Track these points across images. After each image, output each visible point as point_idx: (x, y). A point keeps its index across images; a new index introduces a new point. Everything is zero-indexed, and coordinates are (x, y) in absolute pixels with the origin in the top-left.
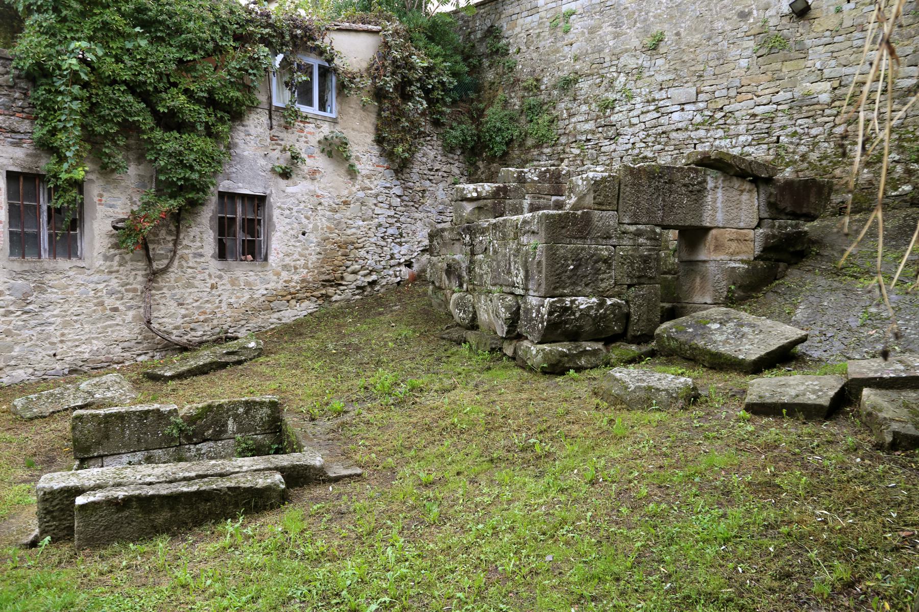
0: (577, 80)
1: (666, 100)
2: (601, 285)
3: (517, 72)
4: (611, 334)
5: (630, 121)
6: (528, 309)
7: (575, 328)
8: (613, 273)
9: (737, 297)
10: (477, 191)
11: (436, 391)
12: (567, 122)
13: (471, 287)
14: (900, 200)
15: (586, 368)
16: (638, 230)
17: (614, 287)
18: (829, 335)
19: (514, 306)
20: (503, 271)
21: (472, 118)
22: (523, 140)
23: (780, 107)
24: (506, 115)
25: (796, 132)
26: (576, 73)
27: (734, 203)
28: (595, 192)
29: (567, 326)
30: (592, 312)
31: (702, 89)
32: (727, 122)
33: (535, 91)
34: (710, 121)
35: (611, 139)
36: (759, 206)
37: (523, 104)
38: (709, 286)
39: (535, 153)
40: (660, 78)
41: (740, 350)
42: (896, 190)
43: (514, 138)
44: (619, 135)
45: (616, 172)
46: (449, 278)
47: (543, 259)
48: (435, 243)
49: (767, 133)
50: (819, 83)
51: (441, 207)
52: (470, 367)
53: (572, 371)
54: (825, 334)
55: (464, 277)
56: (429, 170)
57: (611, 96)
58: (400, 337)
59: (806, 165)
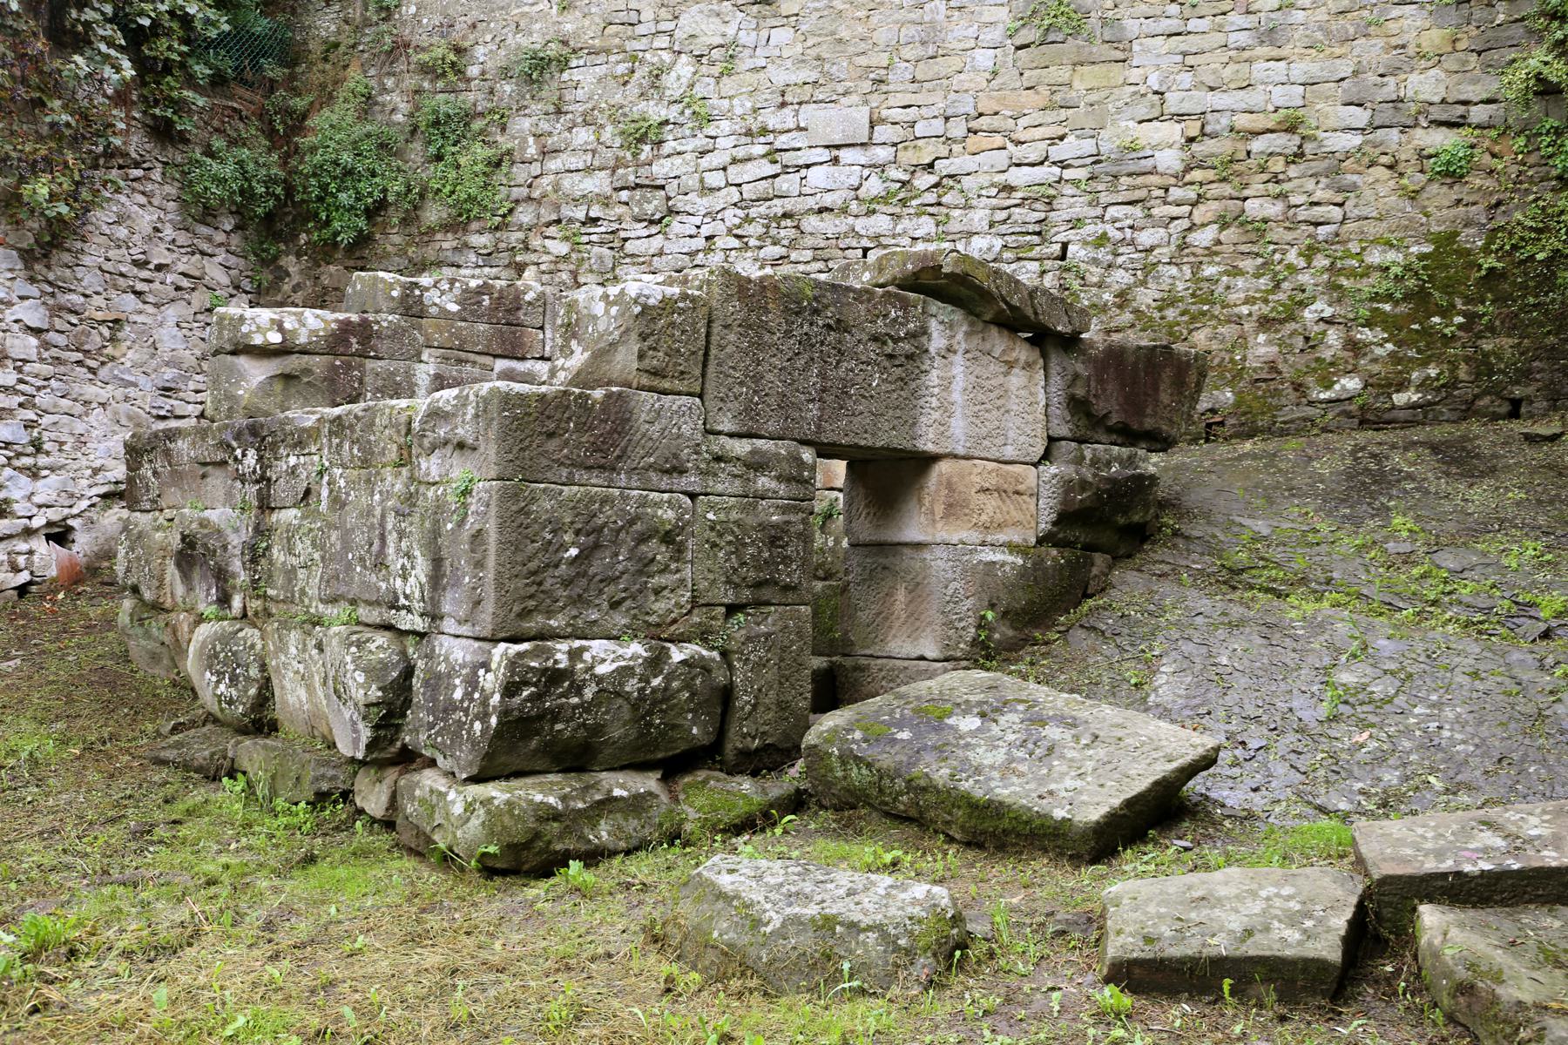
0: (567, 61)
1: (794, 134)
2: (656, 606)
3: (404, 23)
4: (682, 747)
5: (702, 181)
6: (439, 676)
7: (582, 733)
8: (687, 572)
9: (999, 642)
10: (281, 329)
11: (127, 954)
12: (535, 169)
13: (256, 604)
14: (1337, 411)
15: (613, 854)
16: (754, 452)
17: (689, 612)
18: (1253, 744)
19: (395, 666)
20: (362, 559)
21: (271, 133)
22: (416, 208)
23: (1068, 174)
24: (368, 135)
25: (1104, 236)
26: (565, 43)
27: (992, 395)
28: (643, 337)
29: (558, 727)
30: (632, 686)
31: (885, 113)
32: (944, 200)
33: (452, 77)
34: (901, 195)
35: (652, 222)
36: (1047, 405)
37: (418, 109)
38: (932, 613)
39: (445, 245)
40: (780, 77)
41: (1051, 793)
42: (1328, 387)
43: (391, 199)
44: (672, 212)
45: (700, 288)
46: (186, 577)
47: (491, 527)
48: (146, 471)
49: (1039, 233)
50: (1155, 123)
51: (169, 374)
52: (248, 856)
53: (575, 866)
54: (1243, 743)
55: (234, 575)
56: (135, 263)
57: (656, 111)
58: (11, 762)
59: (1127, 317)
